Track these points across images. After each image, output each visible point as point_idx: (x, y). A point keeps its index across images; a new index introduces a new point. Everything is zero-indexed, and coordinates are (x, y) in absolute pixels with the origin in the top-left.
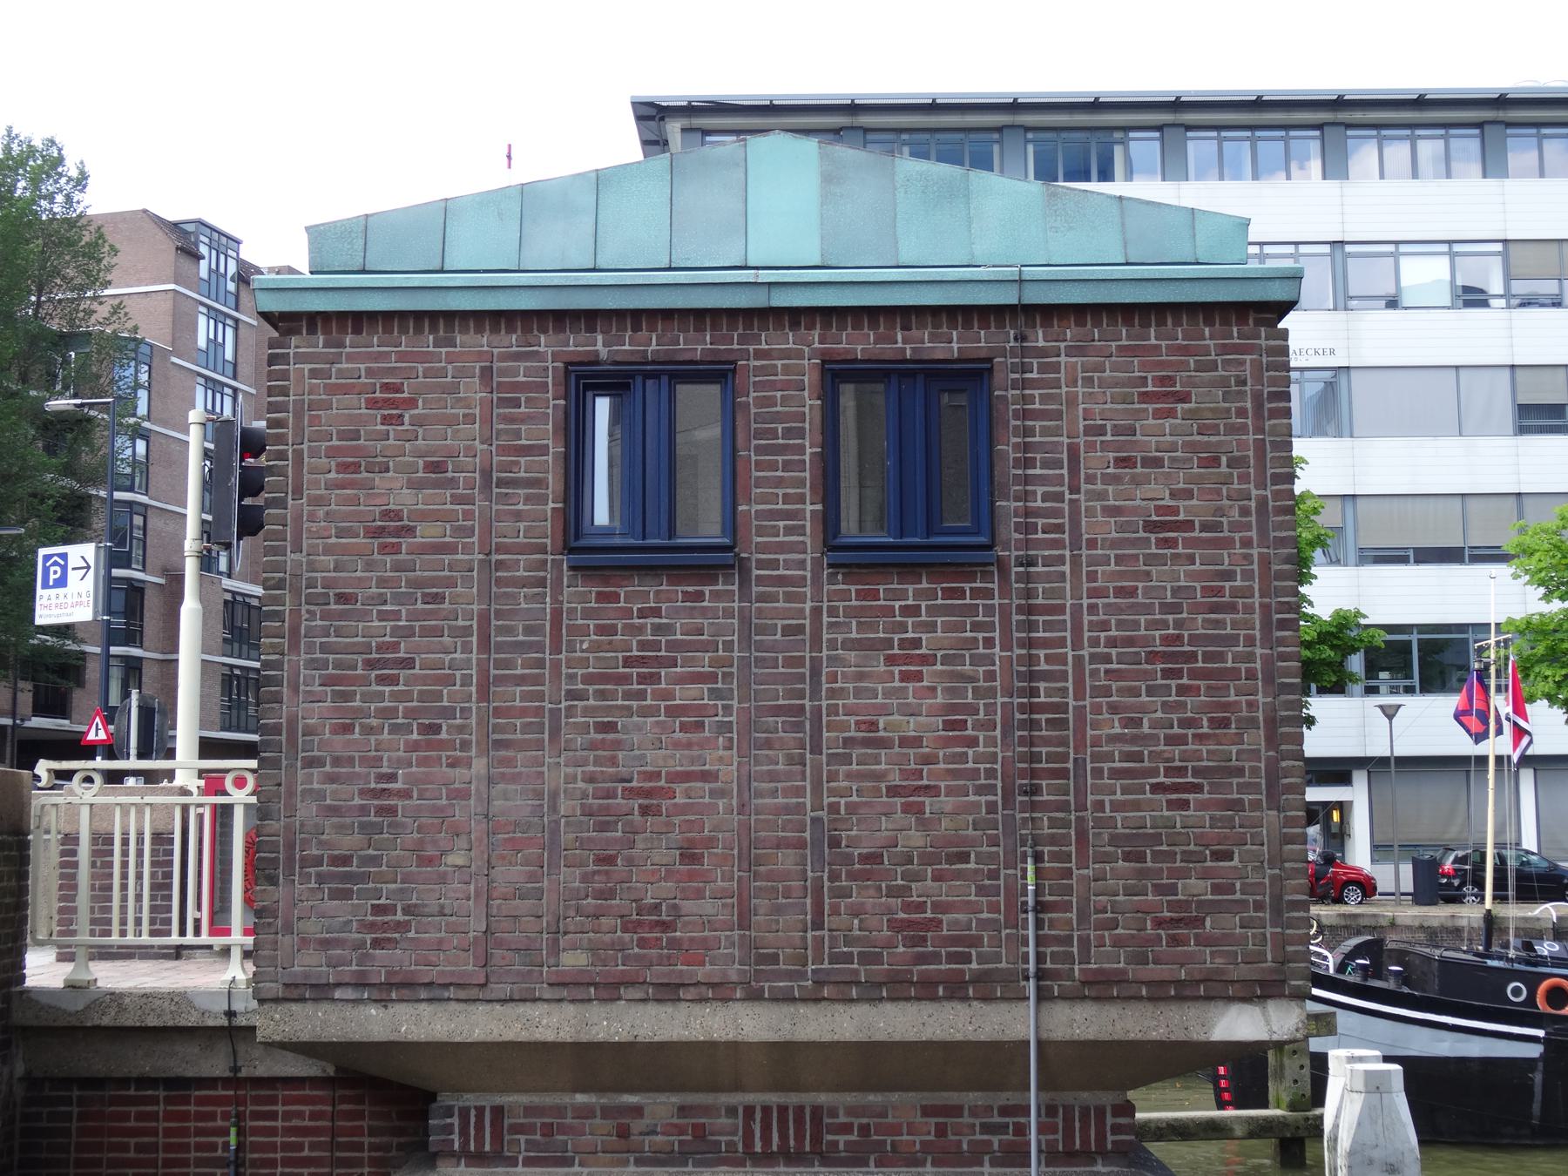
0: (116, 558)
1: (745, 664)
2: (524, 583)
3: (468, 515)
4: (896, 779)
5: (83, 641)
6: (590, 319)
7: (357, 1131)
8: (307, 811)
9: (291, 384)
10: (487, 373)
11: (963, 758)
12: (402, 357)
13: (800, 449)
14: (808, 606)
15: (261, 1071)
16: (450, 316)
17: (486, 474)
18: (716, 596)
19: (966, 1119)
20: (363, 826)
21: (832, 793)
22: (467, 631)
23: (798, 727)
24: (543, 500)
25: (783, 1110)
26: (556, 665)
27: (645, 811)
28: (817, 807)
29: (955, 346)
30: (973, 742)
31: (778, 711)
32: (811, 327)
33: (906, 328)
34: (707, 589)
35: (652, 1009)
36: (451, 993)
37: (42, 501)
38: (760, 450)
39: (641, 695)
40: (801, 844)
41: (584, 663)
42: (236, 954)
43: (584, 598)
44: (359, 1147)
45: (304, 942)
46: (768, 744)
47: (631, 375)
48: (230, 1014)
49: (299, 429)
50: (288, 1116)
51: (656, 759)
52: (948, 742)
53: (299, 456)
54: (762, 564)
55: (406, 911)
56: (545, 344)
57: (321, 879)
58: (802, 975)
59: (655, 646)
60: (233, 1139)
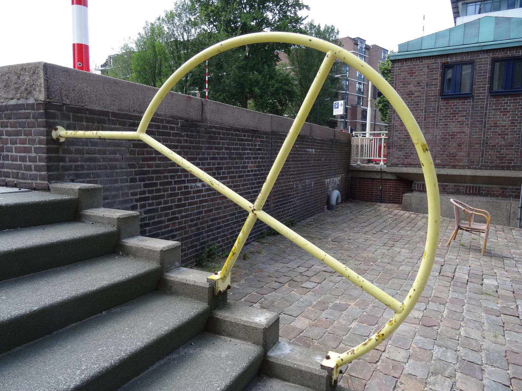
0: (346, 104)
1: (472, 113)
2: (433, 101)
3: (424, 91)
4: (500, 132)
5: (337, 118)
6: (447, 55)
7: (400, 187)
8: (395, 138)
9: (395, 71)
10: (428, 67)
11: (514, 129)
12: (414, 65)
13: (486, 75)
14: (485, 103)
15: (385, 178)
16: (422, 58)
17: (427, 84)
18: (468, 102)
19: (508, 190)
20: (404, 141)
21: (487, 135)
22: (423, 110)
23: (482, 124)
24: (437, 87)
25: (473, 187)
26: (438, 115)
27: (452, 138)
28: (484, 137)
29: (520, 53)
30: (516, 126)
31: (478, 121)
32: (490, 53)
33: (510, 51)
34: (466, 101)
35: (451, 169)
36: (417, 166)
37: (332, 94)
38: (478, 76)
39: (453, 119)
40: (480, 143)
41: (443, 114)
42: (382, 161)
43: (443, 103)
44: (400, 190)
45: (394, 158)
46: (475, 127)
47: (454, 65)
48: (381, 169)
49: (396, 79)
50: (389, 185)
51: (454, 130)
52: (511, 126)
53: (396, 83)
54: (477, 96)
55: (410, 153)
56: (439, 61)
57: (397, 148)
58: (479, 165)
59: (456, 111)
60: (381, 187)
